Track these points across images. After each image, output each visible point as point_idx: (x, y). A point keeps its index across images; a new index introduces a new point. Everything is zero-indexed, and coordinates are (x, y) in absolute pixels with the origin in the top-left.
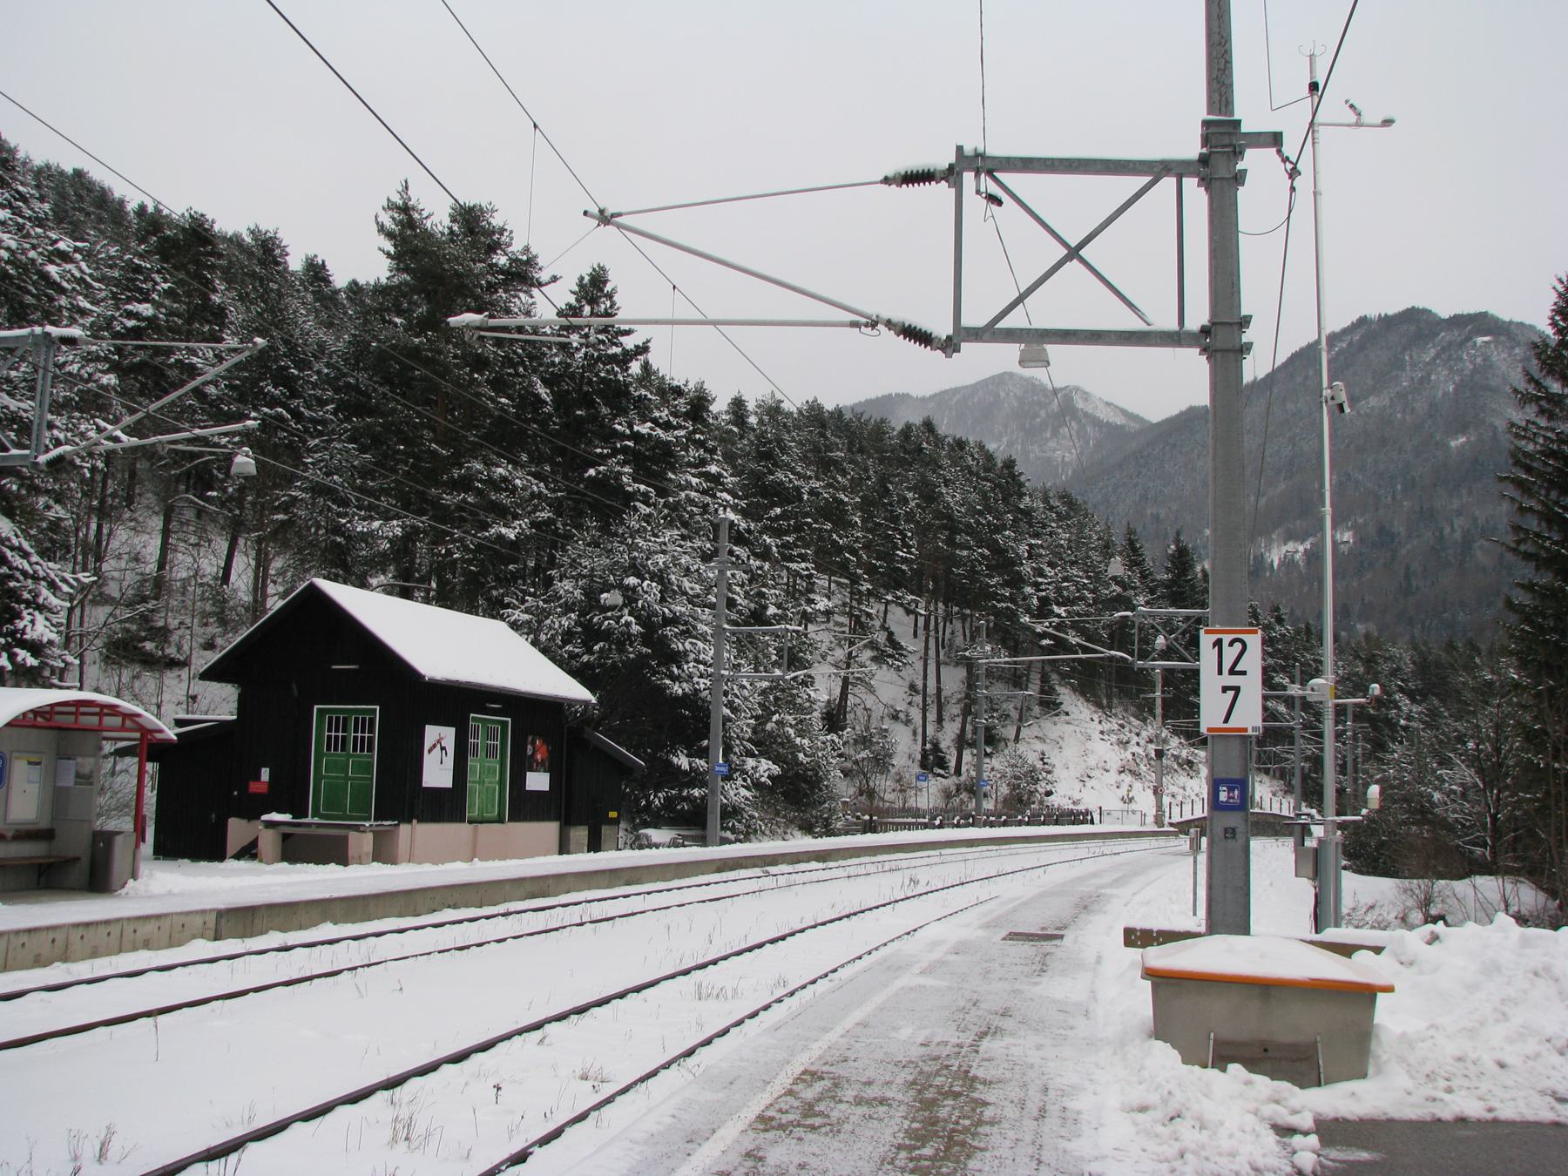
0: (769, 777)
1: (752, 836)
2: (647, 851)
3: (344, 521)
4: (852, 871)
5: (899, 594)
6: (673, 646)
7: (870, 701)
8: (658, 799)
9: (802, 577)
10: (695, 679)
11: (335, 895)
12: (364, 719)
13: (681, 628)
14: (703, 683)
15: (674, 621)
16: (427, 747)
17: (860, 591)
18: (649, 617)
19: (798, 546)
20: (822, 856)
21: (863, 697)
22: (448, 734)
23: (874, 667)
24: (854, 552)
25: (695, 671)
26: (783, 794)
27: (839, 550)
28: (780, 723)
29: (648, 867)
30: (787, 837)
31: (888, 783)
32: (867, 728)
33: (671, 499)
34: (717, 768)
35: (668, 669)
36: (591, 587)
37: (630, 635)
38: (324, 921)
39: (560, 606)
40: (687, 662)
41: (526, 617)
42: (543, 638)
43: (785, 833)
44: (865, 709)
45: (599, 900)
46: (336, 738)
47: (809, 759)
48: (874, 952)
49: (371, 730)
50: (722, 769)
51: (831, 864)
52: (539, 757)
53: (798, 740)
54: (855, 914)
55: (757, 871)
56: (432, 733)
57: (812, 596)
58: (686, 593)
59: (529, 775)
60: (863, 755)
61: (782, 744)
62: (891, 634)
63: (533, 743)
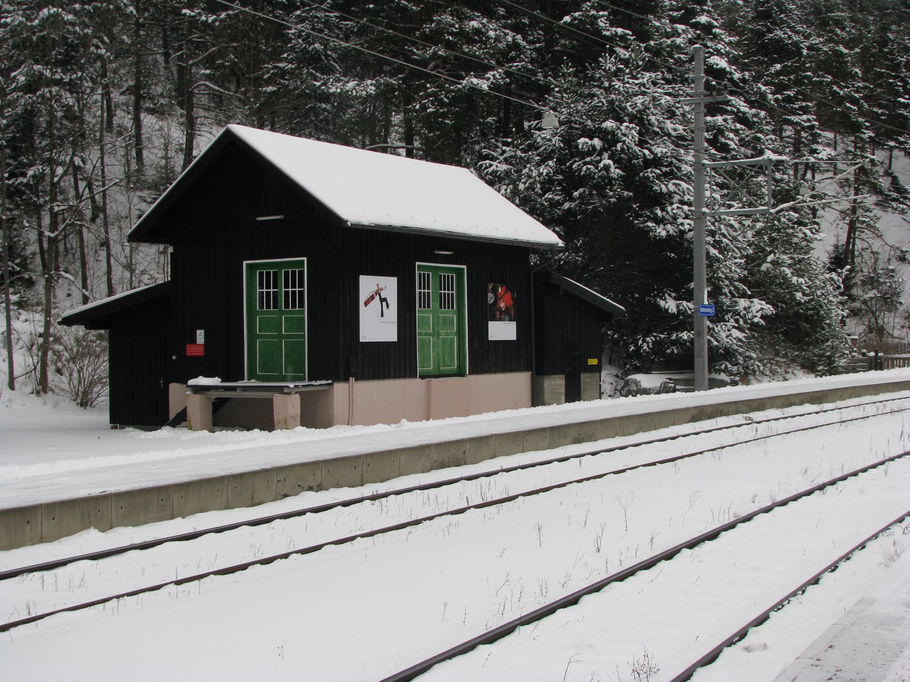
0: (762, 317)
1: (751, 377)
2: (639, 398)
3: (318, 84)
4: (846, 414)
5: (901, 139)
6: (656, 188)
7: (876, 245)
8: (646, 344)
9: (803, 128)
10: (680, 221)
11: (112, 489)
12: (268, 274)
13: (664, 169)
14: (687, 224)
15: (656, 162)
16: (362, 299)
17: (862, 140)
18: (630, 160)
19: (798, 100)
20: (817, 398)
21: (870, 241)
22: (389, 285)
23: (877, 212)
24: (854, 101)
25: (679, 212)
26: (785, 333)
27: (840, 100)
28: (775, 263)
29: (602, 421)
30: (788, 376)
31: (897, 320)
32: (875, 270)
33: (652, 43)
34: (702, 310)
35: (652, 212)
36: (570, 134)
37: (610, 179)
38: (86, 527)
39: (538, 155)
40: (672, 204)
41: (504, 167)
42: (521, 187)
43: (787, 372)
44: (872, 252)
45: (523, 467)
46: (294, 293)
47: (806, 298)
48: (843, 565)
49: (301, 285)
50: (708, 310)
51: (827, 406)
52: (502, 305)
53: (795, 279)
54: (833, 483)
55: (739, 418)
56: (367, 284)
57: (815, 146)
58: (669, 135)
59: (492, 325)
60: (871, 294)
61: (780, 285)
62: (895, 180)
63: (495, 291)
